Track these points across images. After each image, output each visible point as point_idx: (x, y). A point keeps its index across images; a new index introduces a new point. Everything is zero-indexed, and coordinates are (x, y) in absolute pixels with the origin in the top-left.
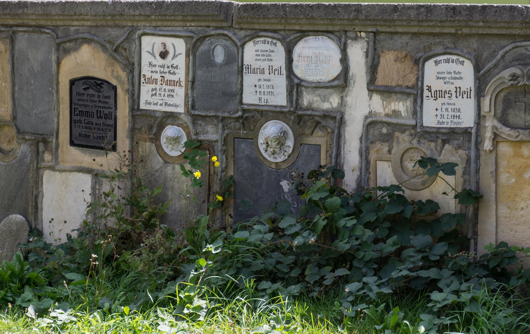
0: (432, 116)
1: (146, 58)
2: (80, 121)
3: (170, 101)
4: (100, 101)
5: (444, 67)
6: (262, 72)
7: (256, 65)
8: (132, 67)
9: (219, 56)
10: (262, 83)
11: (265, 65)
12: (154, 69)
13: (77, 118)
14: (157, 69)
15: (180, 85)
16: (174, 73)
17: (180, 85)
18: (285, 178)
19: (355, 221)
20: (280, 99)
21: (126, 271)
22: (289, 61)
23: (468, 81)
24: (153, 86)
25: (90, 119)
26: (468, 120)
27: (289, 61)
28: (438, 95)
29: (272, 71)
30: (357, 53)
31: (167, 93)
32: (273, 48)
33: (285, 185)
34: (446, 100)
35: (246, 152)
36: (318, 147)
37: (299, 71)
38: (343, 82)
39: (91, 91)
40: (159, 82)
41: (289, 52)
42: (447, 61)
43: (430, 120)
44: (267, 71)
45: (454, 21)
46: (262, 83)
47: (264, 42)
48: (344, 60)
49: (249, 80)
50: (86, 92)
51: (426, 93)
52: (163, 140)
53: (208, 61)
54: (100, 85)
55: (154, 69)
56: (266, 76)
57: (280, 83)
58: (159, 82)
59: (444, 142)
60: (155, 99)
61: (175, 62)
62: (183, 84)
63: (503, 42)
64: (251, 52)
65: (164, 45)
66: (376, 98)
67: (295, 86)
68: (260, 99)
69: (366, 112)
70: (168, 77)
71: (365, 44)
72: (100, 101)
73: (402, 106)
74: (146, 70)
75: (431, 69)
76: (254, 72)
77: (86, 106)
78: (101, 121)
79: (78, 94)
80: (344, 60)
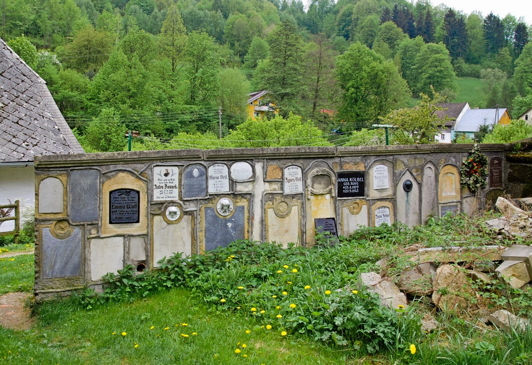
0: (288, 190)
1: (156, 177)
2: (116, 211)
3: (171, 195)
4: (129, 200)
5: (291, 170)
6: (218, 178)
7: (214, 176)
8: (148, 181)
9: (196, 172)
10: (217, 183)
11: (219, 175)
12: (161, 182)
13: (113, 210)
14: (163, 181)
15: (176, 188)
16: (172, 183)
17: (176, 188)
18: (229, 221)
19: (345, 343)
20: (226, 189)
21: (509, 159)
22: (229, 173)
23: (300, 175)
24: (161, 189)
25: (123, 210)
26: (300, 190)
27: (229, 173)
28: (289, 181)
29: (222, 177)
30: (259, 166)
31: (168, 192)
32: (222, 168)
33: (230, 225)
34: (292, 182)
35: (211, 214)
36: (243, 207)
37: (233, 176)
38: (253, 180)
39: (123, 196)
40: (164, 187)
41: (229, 169)
42: (292, 168)
43: (287, 191)
44: (220, 178)
45: (343, 28)
46: (217, 183)
47: (218, 166)
48: (254, 171)
49: (211, 182)
50: (120, 197)
51: (285, 181)
52: (167, 213)
53: (190, 175)
54: (129, 192)
55: (161, 182)
56: (220, 179)
57: (226, 182)
58: (164, 187)
59: (293, 198)
60: (162, 195)
61: (173, 178)
62: (177, 187)
63: (311, 160)
64: (212, 171)
65: (167, 170)
66: (267, 184)
67: (233, 183)
68: (217, 190)
69: (263, 190)
70: (168, 185)
71: (262, 164)
72: (129, 200)
73: (276, 187)
74: (156, 182)
75: (286, 171)
76: (214, 178)
77: (120, 203)
78: (130, 210)
79: (115, 198)
80: (254, 171)
